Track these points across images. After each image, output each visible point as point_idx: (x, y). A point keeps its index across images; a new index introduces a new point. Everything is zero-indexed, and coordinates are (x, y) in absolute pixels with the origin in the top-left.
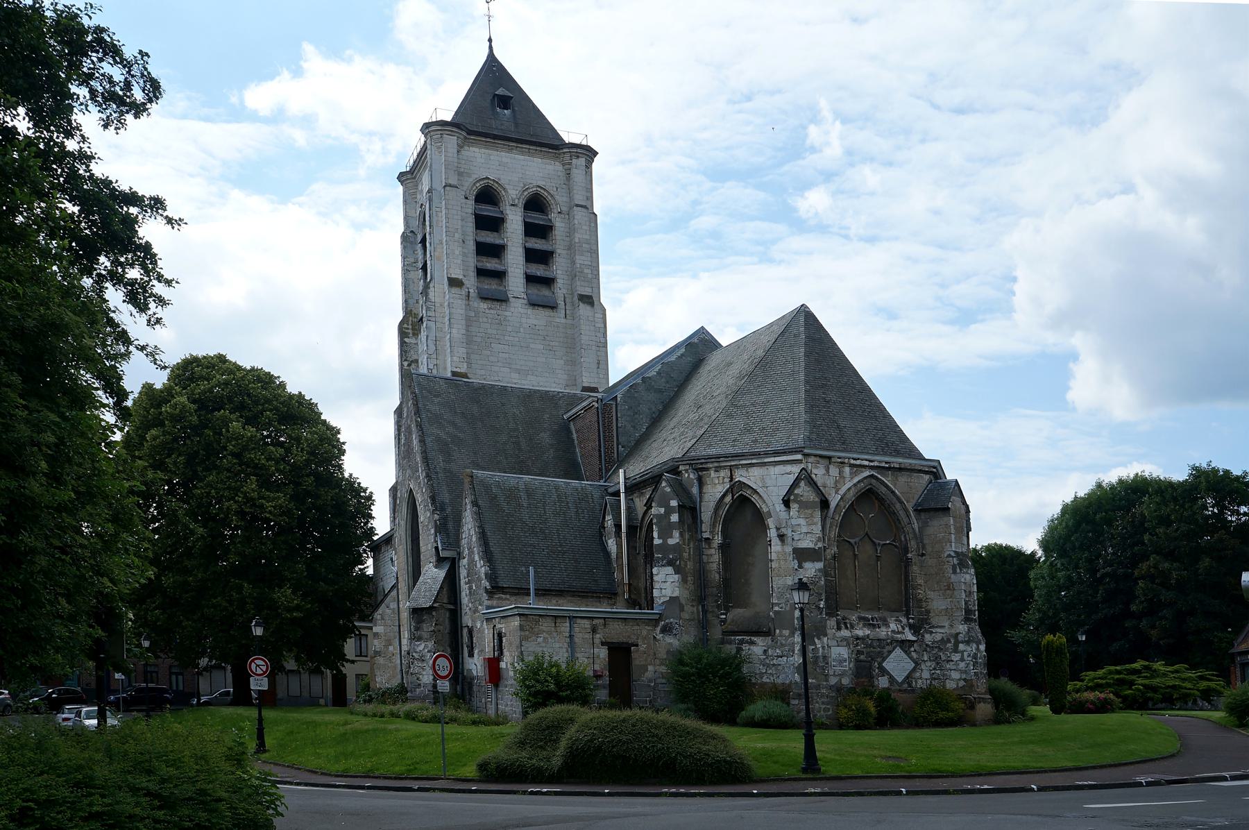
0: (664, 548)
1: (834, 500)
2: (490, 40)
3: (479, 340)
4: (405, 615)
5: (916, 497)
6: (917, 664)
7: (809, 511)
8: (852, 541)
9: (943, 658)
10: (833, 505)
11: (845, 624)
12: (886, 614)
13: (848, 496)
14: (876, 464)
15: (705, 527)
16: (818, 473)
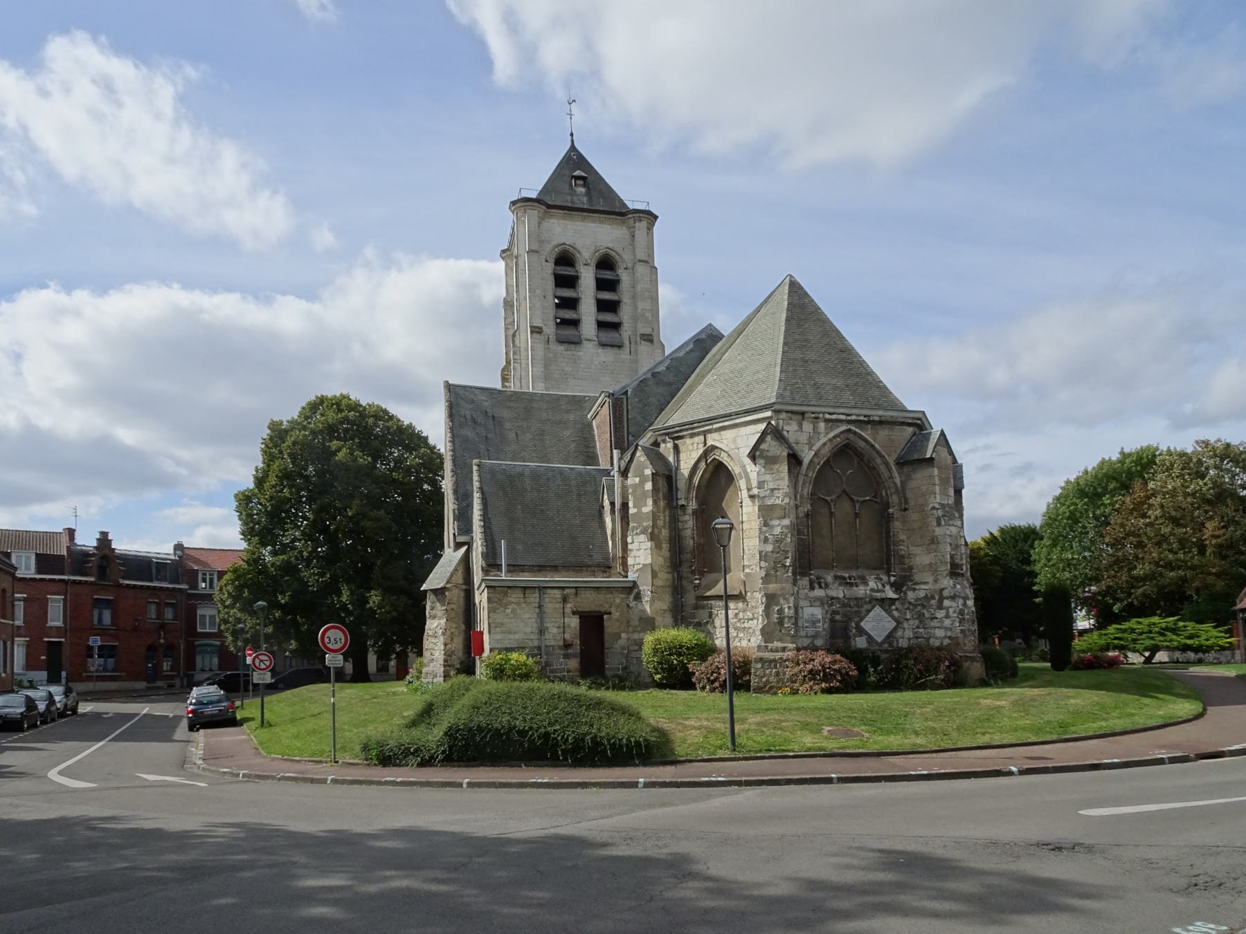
1: (807, 456)
2: (572, 135)
6: (899, 623)
8: (828, 499)
9: (927, 615)
10: (806, 461)
11: (820, 584)
12: (865, 572)
14: (854, 418)
15: (681, 494)
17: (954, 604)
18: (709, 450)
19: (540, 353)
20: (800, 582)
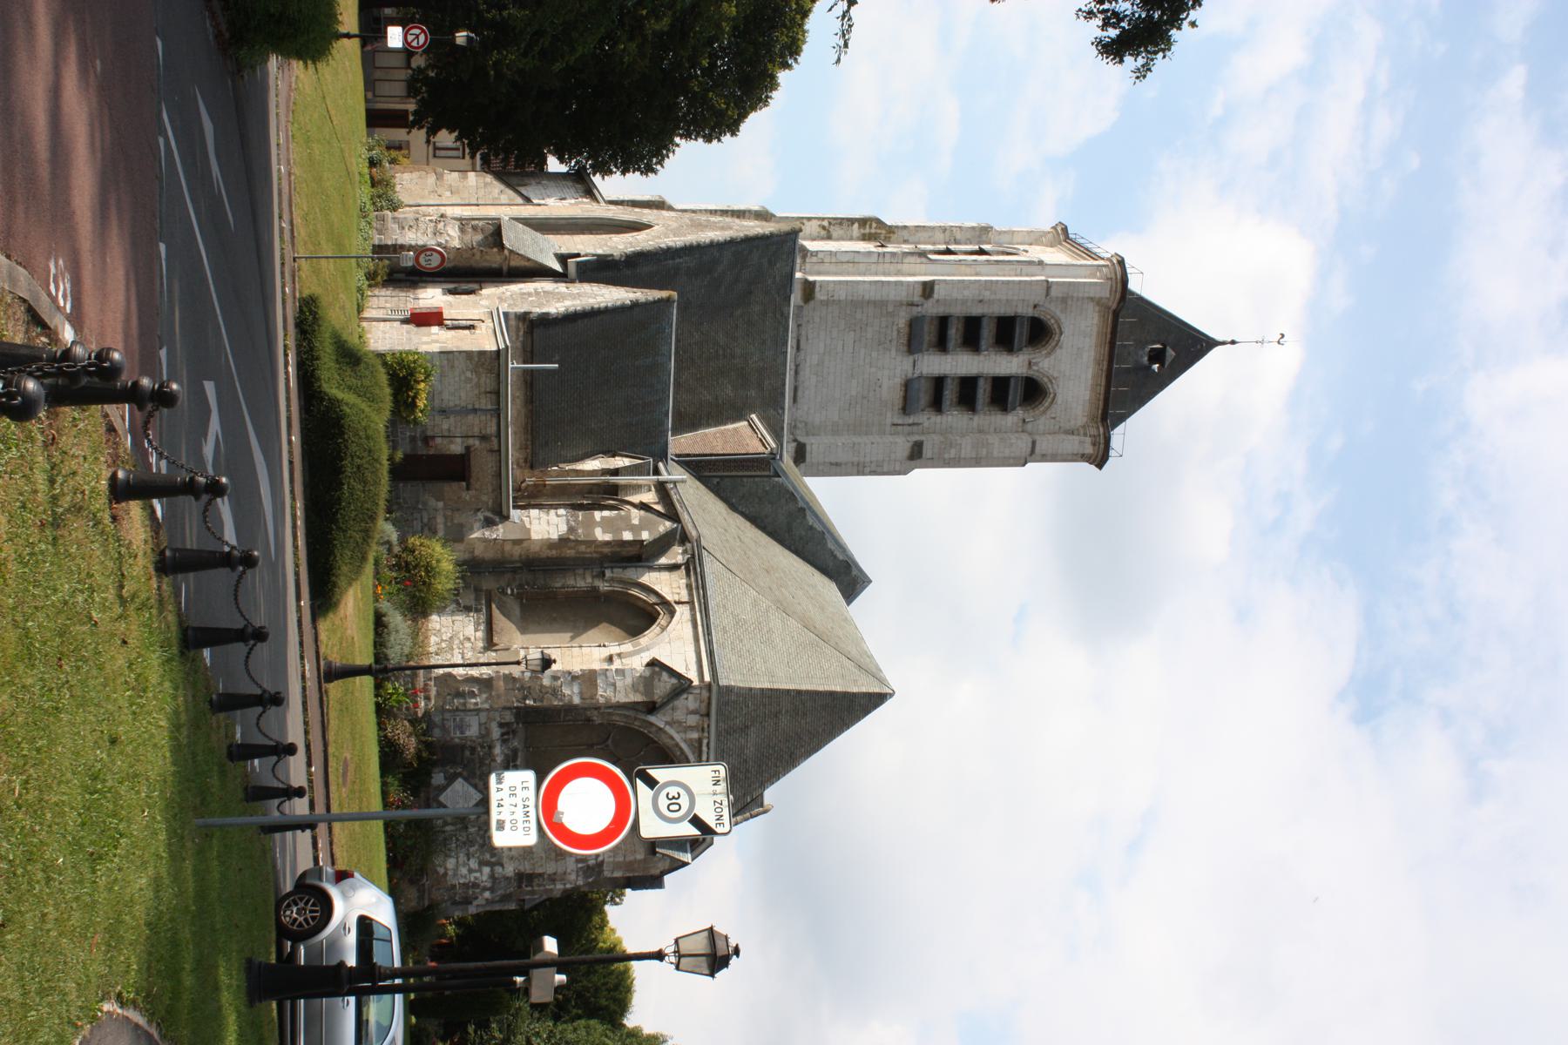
0: (591, 524)
1: (658, 720)
2: (1233, 342)
3: (859, 316)
4: (492, 212)
10: (652, 719)
15: (618, 573)
16: (690, 701)
19: (893, 295)
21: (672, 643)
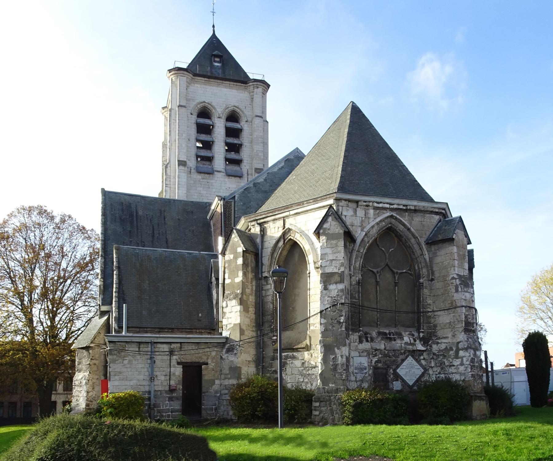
1: (359, 235)
2: (214, 26)
5: (428, 233)
7: (334, 242)
8: (375, 271)
9: (447, 364)
10: (358, 241)
12: (401, 330)
13: (371, 233)
14: (395, 206)
15: (265, 268)
16: (347, 213)
17: (468, 354)
18: (286, 232)
19: (184, 180)
20: (352, 337)
21: (304, 224)
